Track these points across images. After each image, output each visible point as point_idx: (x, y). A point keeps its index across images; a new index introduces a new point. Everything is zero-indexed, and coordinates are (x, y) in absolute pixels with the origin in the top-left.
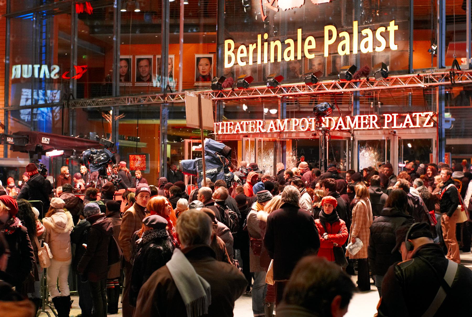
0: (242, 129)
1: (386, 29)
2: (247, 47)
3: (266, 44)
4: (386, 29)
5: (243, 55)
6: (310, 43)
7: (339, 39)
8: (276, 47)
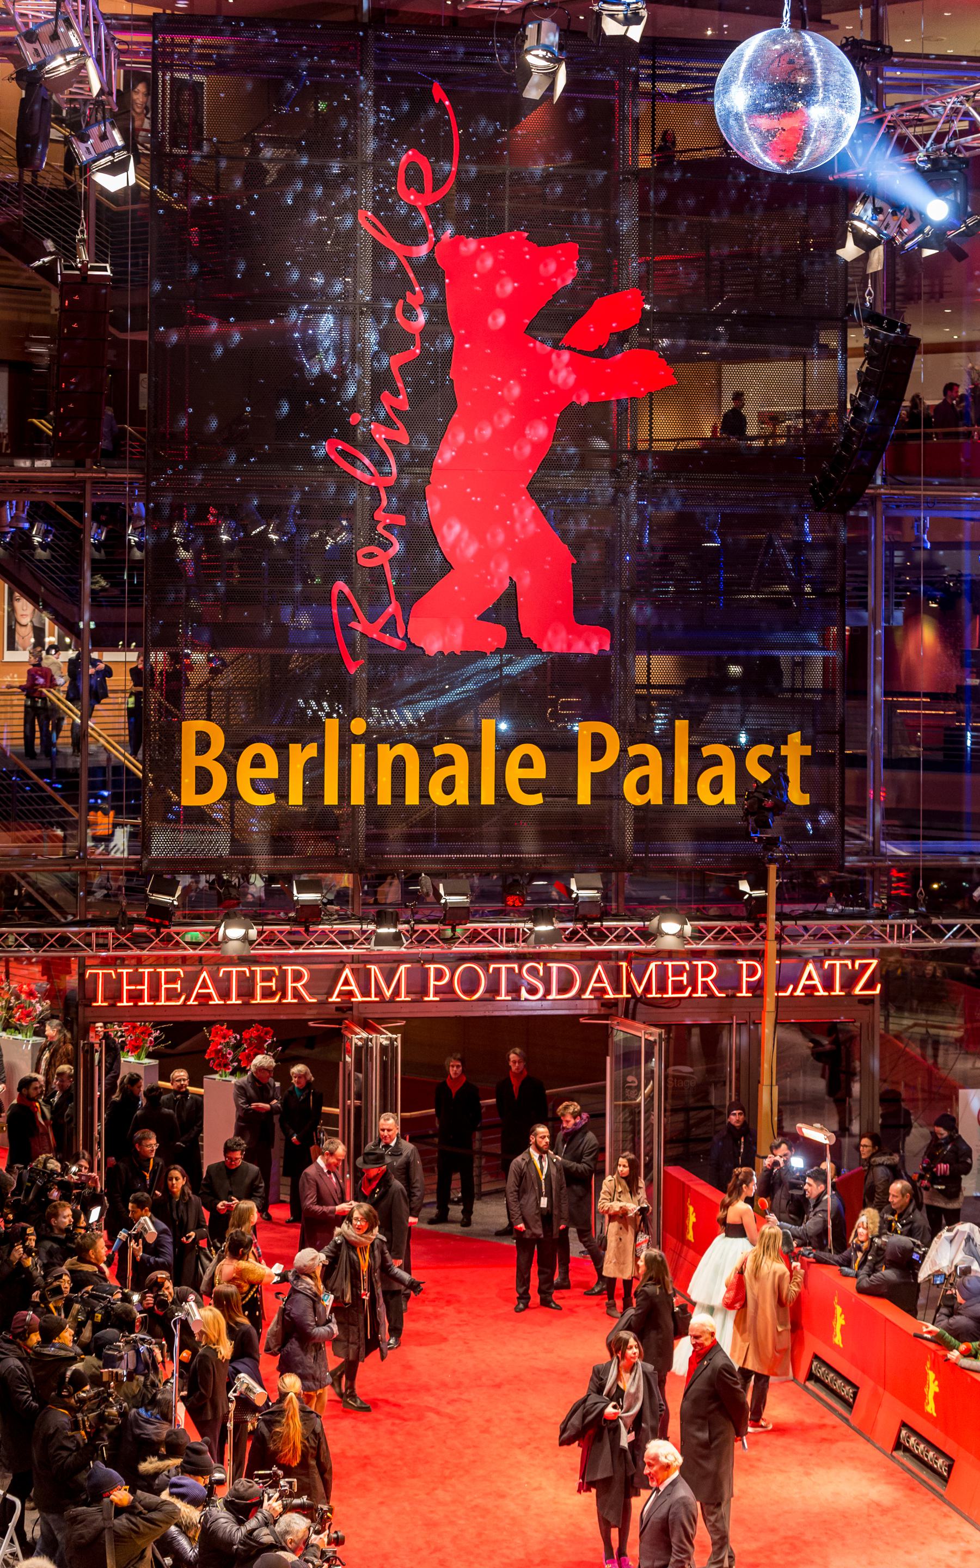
0: (225, 995)
1: (777, 749)
2: (282, 750)
3: (358, 752)
4: (777, 749)
5: (259, 773)
6: (526, 762)
7: (625, 764)
8: (399, 765)
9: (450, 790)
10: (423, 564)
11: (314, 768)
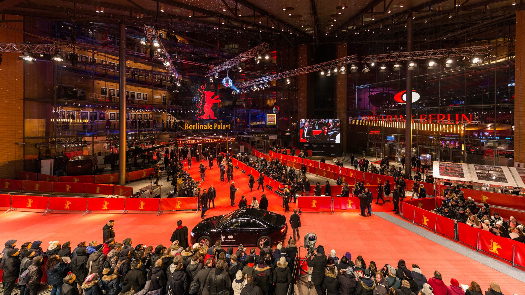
9: (205, 128)
10: (203, 113)
11: (195, 127)
